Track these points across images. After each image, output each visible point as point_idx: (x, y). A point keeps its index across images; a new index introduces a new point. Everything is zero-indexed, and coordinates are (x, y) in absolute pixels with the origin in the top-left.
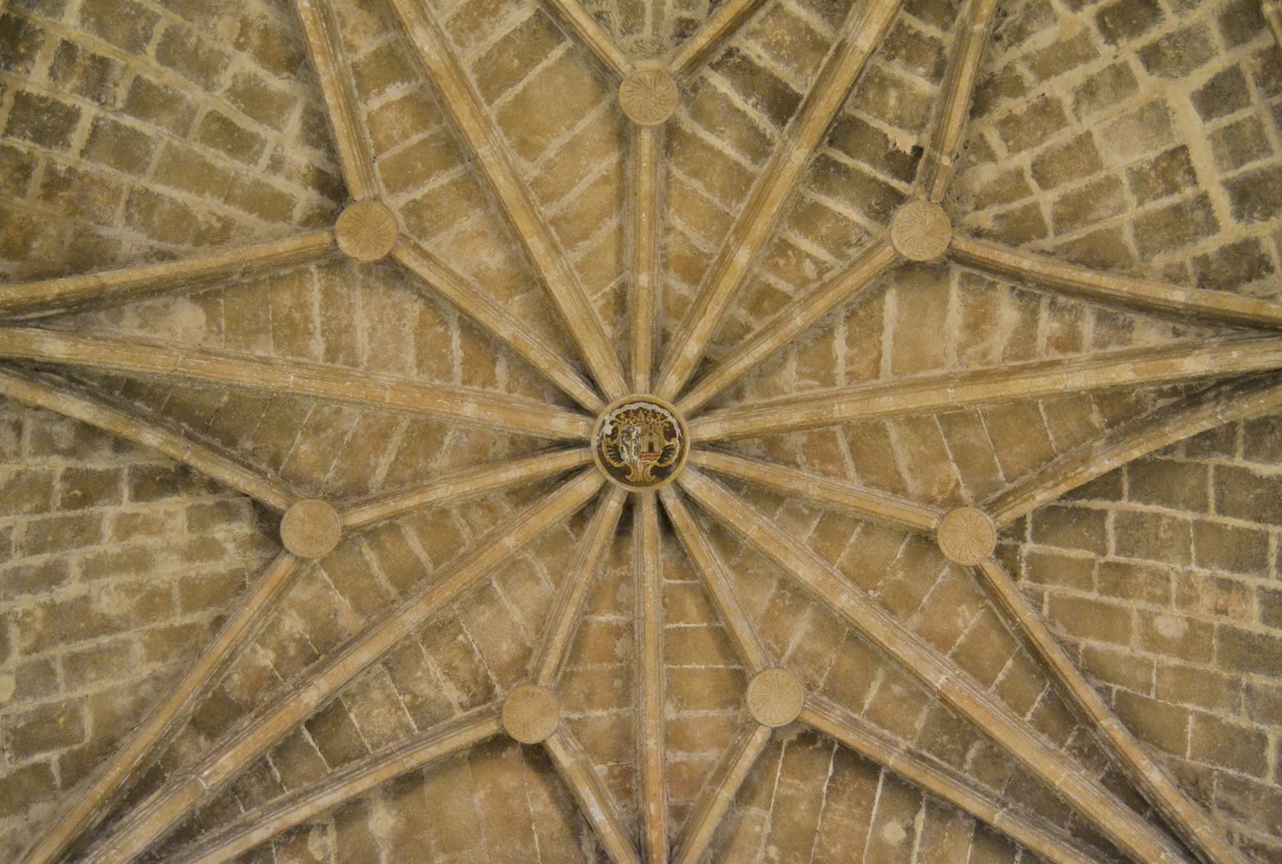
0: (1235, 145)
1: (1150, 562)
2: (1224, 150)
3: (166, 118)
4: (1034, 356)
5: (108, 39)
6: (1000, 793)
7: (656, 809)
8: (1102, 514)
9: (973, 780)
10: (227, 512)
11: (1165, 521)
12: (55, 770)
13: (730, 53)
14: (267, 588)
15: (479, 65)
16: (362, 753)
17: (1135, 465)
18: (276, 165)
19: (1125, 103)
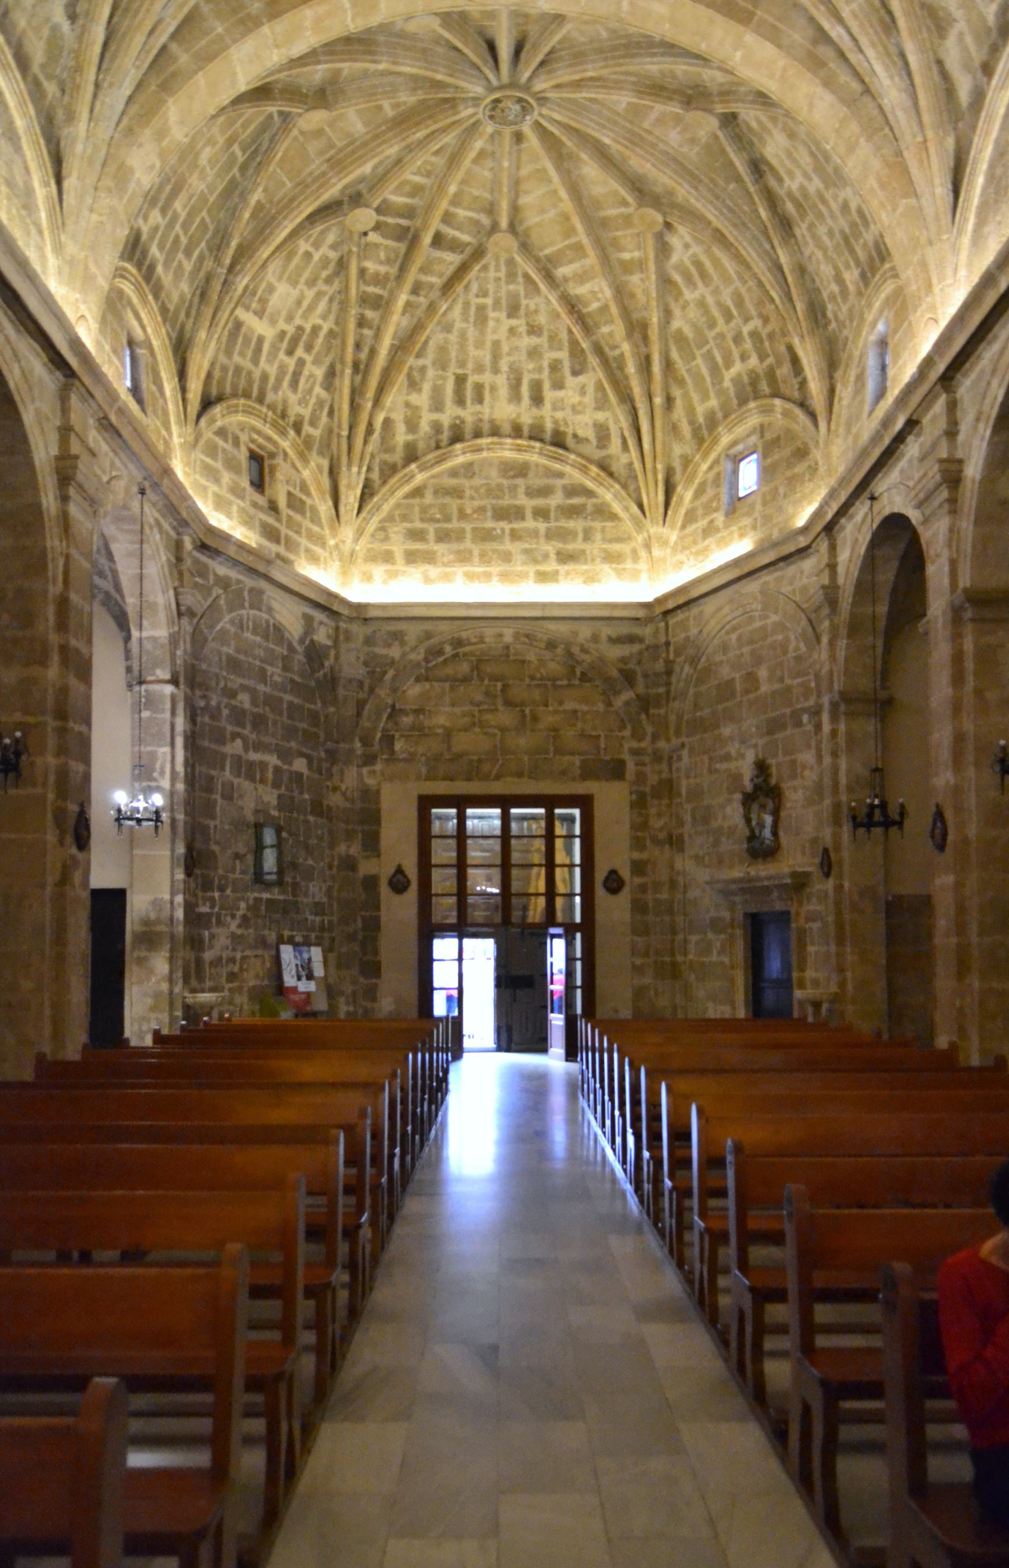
18: (687, 246)
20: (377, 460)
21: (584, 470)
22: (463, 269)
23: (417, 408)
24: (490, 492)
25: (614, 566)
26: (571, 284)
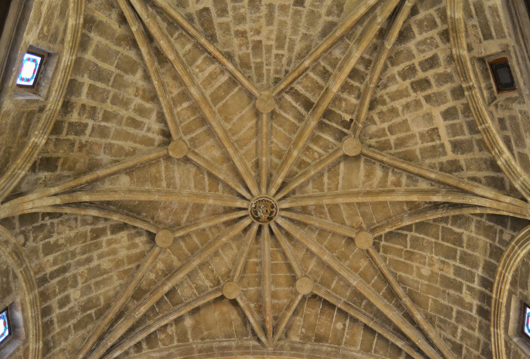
0: (453, 130)
1: (420, 252)
2: (450, 131)
3: (114, 121)
4: (386, 187)
5: (95, 101)
6: (372, 316)
7: (269, 319)
8: (406, 236)
9: (364, 311)
10: (139, 233)
11: (425, 240)
12: (93, 315)
13: (291, 89)
14: (152, 257)
15: (211, 95)
16: (182, 302)
17: (416, 224)
19: (419, 112)
26: (218, 70)
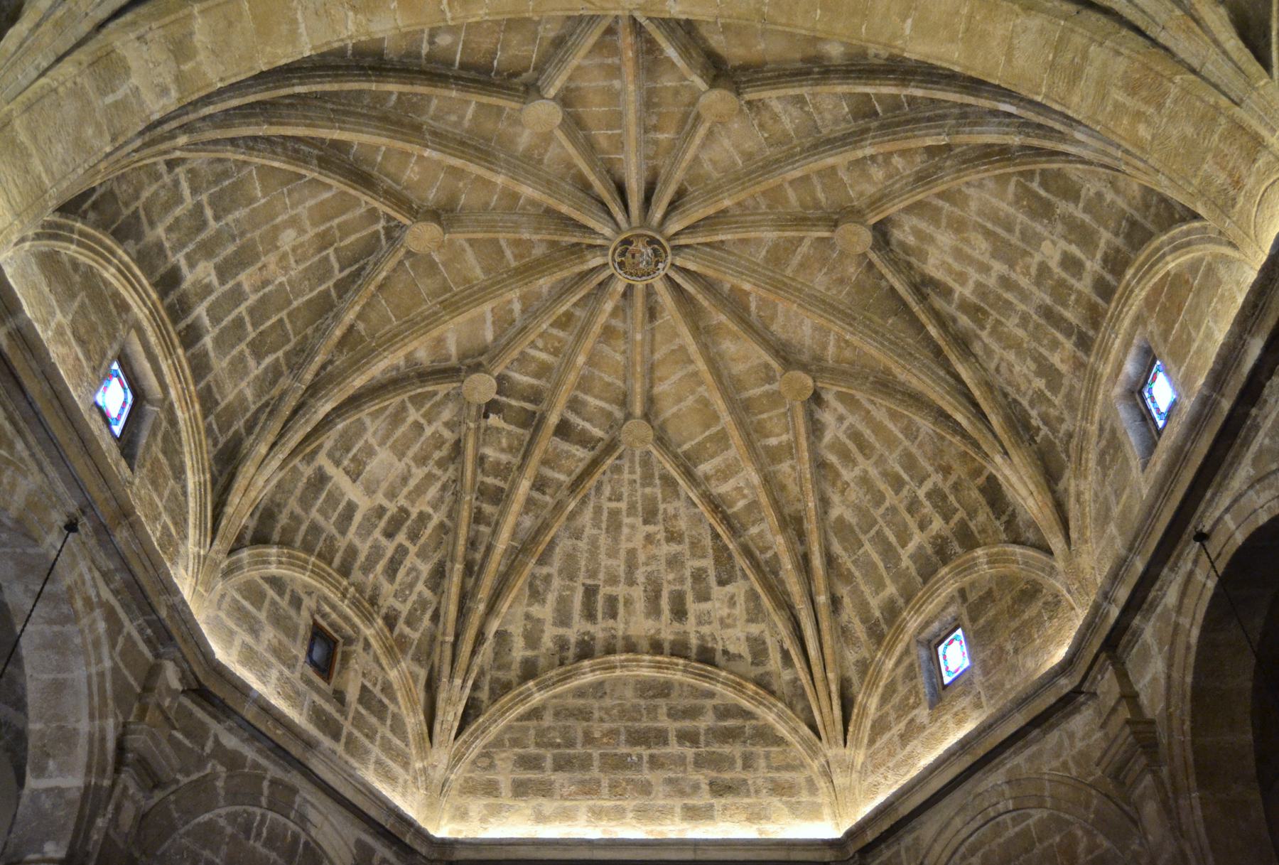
18: (841, 419)
20: (488, 677)
21: (739, 688)
22: (595, 464)
23: (539, 620)
24: (623, 713)
25: (784, 798)
26: (713, 483)
